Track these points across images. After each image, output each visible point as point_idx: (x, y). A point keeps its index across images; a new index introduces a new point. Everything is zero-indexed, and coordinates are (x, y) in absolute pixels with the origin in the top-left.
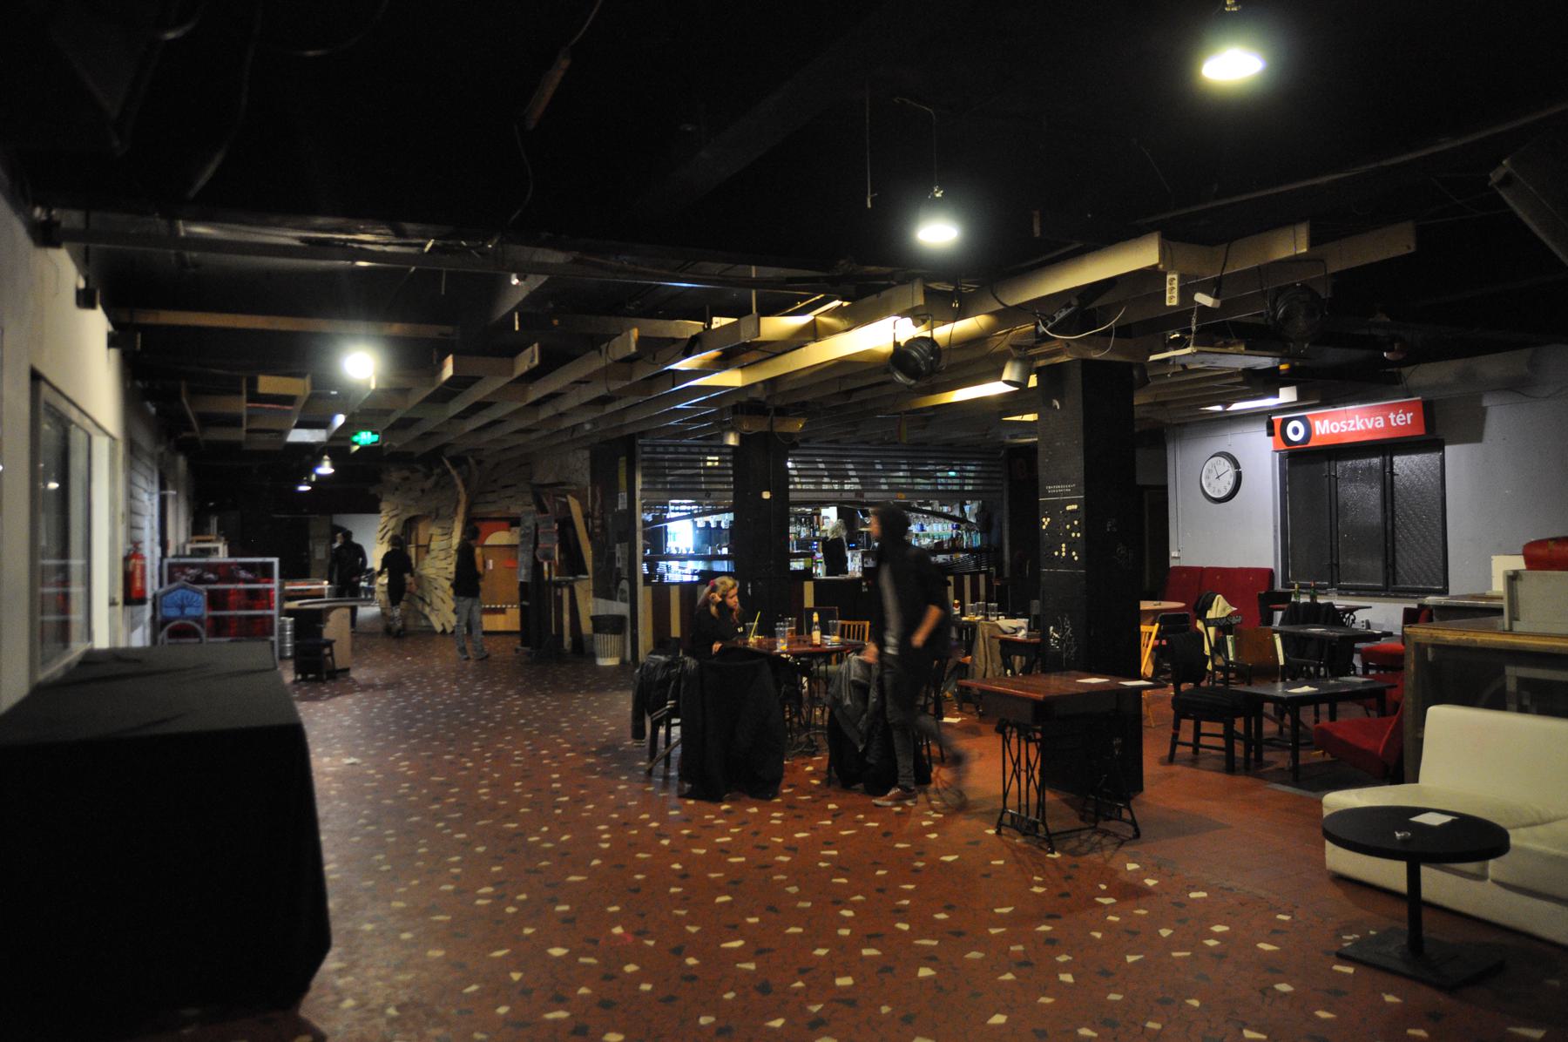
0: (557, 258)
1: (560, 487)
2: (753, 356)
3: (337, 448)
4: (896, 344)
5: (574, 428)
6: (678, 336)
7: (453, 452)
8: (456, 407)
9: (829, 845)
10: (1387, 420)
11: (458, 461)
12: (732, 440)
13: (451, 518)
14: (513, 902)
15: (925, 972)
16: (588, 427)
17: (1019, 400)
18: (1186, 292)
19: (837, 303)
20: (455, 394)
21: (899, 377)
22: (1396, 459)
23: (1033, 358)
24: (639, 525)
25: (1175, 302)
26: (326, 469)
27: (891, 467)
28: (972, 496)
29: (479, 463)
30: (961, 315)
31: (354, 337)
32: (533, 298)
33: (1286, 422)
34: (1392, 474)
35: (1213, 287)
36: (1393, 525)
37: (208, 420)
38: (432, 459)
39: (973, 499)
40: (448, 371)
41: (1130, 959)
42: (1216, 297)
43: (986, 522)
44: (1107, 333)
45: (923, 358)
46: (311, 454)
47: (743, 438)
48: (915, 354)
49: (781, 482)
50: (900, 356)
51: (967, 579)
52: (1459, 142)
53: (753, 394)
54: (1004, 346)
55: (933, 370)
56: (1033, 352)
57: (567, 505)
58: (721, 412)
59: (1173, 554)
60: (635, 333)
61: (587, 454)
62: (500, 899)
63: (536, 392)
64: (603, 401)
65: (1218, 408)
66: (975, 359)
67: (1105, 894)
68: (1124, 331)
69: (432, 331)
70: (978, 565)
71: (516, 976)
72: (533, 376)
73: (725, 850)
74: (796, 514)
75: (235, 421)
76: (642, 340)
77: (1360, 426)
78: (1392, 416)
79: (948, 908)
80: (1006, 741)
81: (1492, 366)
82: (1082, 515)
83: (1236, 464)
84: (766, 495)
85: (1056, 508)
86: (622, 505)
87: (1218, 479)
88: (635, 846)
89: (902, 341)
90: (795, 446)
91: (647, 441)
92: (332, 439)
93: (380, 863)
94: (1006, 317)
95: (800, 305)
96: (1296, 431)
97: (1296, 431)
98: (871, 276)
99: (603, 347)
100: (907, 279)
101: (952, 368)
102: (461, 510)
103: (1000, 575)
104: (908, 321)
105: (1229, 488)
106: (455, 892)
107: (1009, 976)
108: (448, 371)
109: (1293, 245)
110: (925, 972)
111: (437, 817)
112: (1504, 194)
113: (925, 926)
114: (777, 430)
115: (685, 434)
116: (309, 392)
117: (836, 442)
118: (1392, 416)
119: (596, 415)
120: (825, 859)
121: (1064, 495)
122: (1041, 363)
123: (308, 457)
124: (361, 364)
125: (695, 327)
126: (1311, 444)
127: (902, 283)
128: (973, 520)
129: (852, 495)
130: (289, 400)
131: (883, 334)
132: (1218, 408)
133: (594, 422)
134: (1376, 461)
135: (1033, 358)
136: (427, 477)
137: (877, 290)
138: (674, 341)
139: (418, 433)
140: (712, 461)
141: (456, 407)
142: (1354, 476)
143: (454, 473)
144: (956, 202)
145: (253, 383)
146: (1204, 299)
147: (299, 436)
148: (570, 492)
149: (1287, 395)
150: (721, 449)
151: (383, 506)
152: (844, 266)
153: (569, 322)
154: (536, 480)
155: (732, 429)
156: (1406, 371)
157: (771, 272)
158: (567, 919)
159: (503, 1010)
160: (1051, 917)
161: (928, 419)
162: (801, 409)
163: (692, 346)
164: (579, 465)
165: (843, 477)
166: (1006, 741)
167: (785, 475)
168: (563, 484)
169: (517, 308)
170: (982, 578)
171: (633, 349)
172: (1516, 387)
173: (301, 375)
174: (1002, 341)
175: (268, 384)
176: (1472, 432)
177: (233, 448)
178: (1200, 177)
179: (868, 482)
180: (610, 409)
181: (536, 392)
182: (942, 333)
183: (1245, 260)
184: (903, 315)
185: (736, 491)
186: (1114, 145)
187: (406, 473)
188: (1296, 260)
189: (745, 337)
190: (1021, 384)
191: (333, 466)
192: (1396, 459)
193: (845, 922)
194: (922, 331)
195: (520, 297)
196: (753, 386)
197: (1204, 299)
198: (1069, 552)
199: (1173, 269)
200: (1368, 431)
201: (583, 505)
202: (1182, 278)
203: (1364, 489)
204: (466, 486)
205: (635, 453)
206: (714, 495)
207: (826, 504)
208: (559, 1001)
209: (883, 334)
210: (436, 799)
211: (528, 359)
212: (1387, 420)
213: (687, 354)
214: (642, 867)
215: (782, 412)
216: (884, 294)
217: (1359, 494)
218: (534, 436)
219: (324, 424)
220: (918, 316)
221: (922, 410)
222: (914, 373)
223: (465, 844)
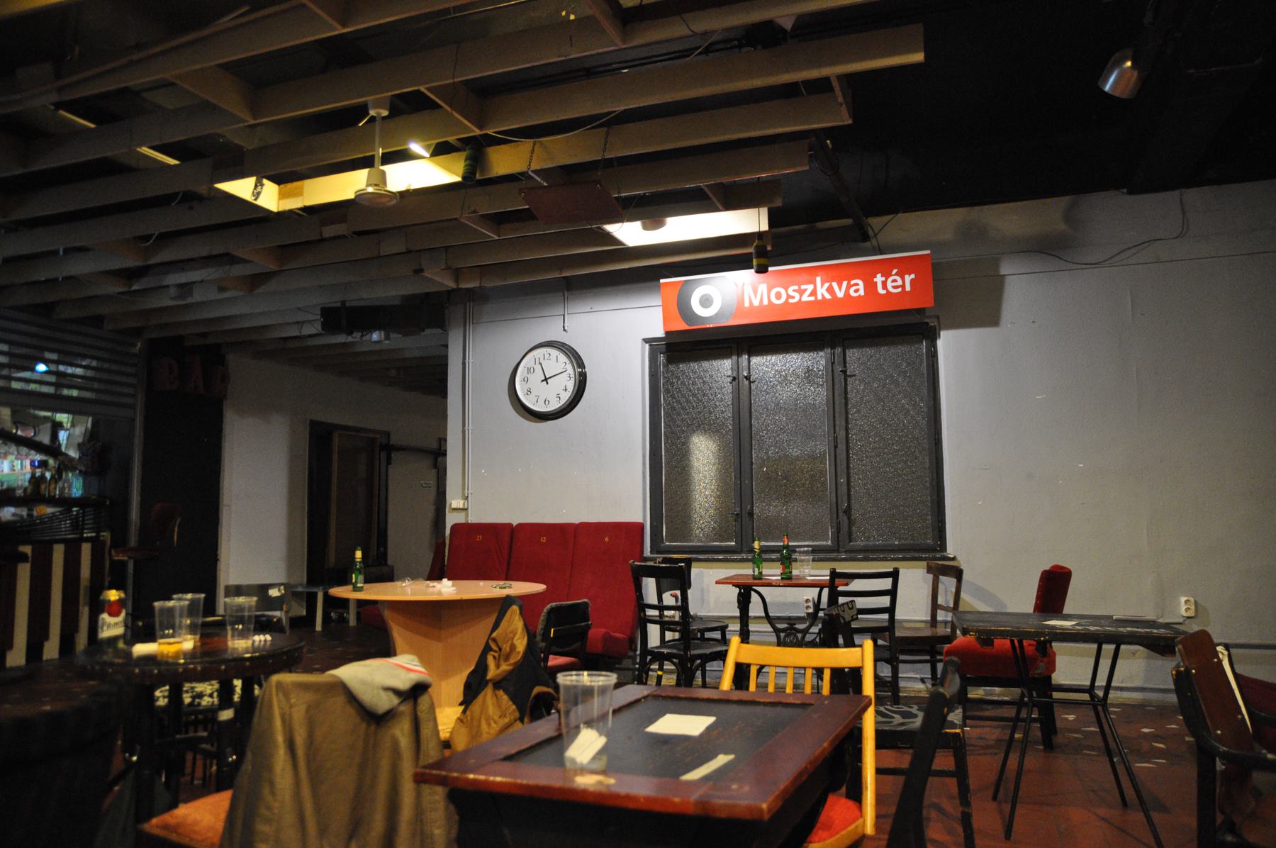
10: (870, 286)
43: (98, 456)
51: (58, 553)
70: (77, 526)
77: (822, 292)
78: (879, 279)
80: (796, 560)
81: (1008, 219)
103: (120, 542)
118: (879, 279)
128: (73, 454)
166: (796, 560)
170: (86, 549)
172: (1049, 248)
176: (984, 311)
212: (870, 286)
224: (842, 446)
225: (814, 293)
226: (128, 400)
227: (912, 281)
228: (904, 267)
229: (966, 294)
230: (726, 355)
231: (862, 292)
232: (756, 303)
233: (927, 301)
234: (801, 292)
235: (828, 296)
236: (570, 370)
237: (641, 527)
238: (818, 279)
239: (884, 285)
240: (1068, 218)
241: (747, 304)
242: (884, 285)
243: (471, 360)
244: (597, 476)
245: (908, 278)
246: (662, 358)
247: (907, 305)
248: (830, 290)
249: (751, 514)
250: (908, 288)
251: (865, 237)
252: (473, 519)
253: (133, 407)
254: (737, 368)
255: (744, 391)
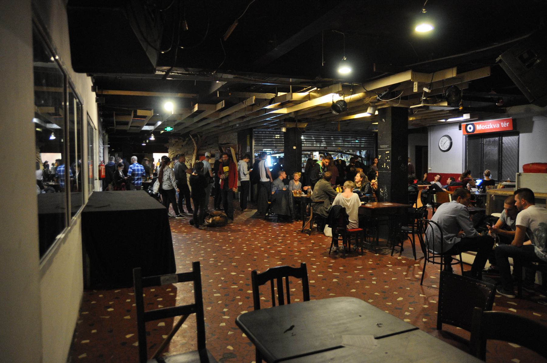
0: (230, 76)
1: (227, 145)
2: (291, 104)
3: (156, 132)
4: (333, 102)
5: (233, 126)
6: (267, 98)
7: (193, 133)
8: (196, 119)
9: (311, 251)
10: (500, 125)
11: (194, 136)
12: (284, 130)
13: (192, 155)
14: (220, 262)
15: (335, 280)
16: (237, 125)
17: (373, 118)
18: (420, 87)
19: (316, 88)
20: (197, 115)
21: (334, 112)
22: (504, 138)
23: (377, 106)
24: (253, 157)
25: (416, 91)
26: (152, 138)
27: (336, 139)
28: (364, 149)
29: (201, 136)
30: (354, 93)
31: (167, 97)
32: (223, 87)
33: (467, 125)
34: (502, 143)
35: (429, 86)
36: (502, 160)
37: (119, 123)
38: (186, 135)
39: (364, 150)
40: (196, 109)
41: (393, 279)
42: (429, 89)
44: (398, 99)
45: (341, 107)
46: (149, 133)
47: (287, 129)
48: (339, 105)
49: (299, 143)
50: (334, 106)
52: (500, 45)
53: (291, 116)
54: (368, 102)
55: (344, 110)
56: (376, 104)
57: (230, 150)
58: (280, 121)
59: (429, 168)
60: (254, 98)
61: (236, 134)
62: (216, 261)
63: (222, 115)
64: (243, 117)
65: (444, 121)
66: (359, 106)
67: (390, 264)
68: (404, 98)
69: (191, 96)
71: (223, 278)
72: (222, 110)
73: (280, 251)
74: (305, 154)
75: (126, 123)
76: (256, 99)
77: (491, 127)
78: (502, 124)
79: (343, 266)
82: (390, 155)
83: (450, 139)
84: (295, 148)
85: (383, 152)
86: (248, 151)
87: (444, 144)
88: (254, 250)
89: (335, 101)
90: (304, 132)
91: (256, 130)
92: (156, 129)
93: (181, 253)
94: (369, 93)
95: (305, 89)
96: (470, 128)
97: (470, 128)
98: (326, 82)
99: (244, 101)
100: (337, 82)
101: (353, 108)
102: (195, 152)
104: (338, 95)
105: (448, 147)
106: (204, 260)
107: (358, 282)
108: (196, 109)
109: (452, 74)
110: (335, 280)
111: (195, 242)
112: (501, 65)
113: (336, 269)
114: (298, 127)
115: (269, 128)
116: (153, 115)
117: (318, 130)
118: (502, 124)
119: (241, 121)
120: (309, 254)
121: (386, 148)
122: (379, 107)
123: (146, 135)
124: (169, 106)
125: (272, 95)
126: (475, 133)
127: (335, 84)
129: (323, 148)
130: (145, 117)
131: (331, 98)
132: (444, 121)
133: (239, 124)
134: (497, 139)
135: (377, 106)
136: (184, 141)
137: (328, 86)
138: (266, 100)
139: (183, 127)
140: (277, 136)
141: (196, 119)
142: (489, 144)
143: (193, 140)
144: (351, 60)
145: (135, 112)
146: (426, 90)
147: (146, 128)
148: (231, 146)
149: (466, 116)
150: (280, 133)
151: (169, 150)
152: (318, 78)
153: (233, 95)
154: (220, 142)
155: (284, 126)
156: (508, 108)
157: (295, 80)
158: (235, 266)
159: (220, 285)
160: (372, 269)
161: (348, 123)
162: (306, 120)
163: (271, 101)
164: (234, 138)
165: (321, 142)
167: (301, 142)
168: (229, 144)
169: (218, 90)
171: (254, 102)
173: (150, 110)
174: (368, 100)
175: (140, 112)
176: (529, 130)
177: (125, 131)
178: (420, 57)
179: (329, 143)
180: (245, 120)
181: (222, 115)
182: (348, 98)
183: (438, 77)
184: (337, 93)
185: (285, 146)
186: (385, 52)
187: (177, 140)
188: (453, 78)
189: (288, 99)
190: (373, 114)
191: (155, 138)
192: (504, 138)
193: (314, 269)
194: (342, 98)
195: (219, 86)
196: (290, 113)
197: (426, 90)
198: (386, 166)
199: (415, 81)
200: (494, 129)
201: (235, 150)
202: (419, 83)
203: (492, 148)
204: (197, 144)
205: (249, 133)
206: (278, 147)
207: (315, 151)
208: (235, 284)
209: (331, 98)
210: (194, 238)
211: (221, 105)
212: (500, 125)
213: (270, 104)
214: (256, 255)
215: (300, 121)
216: (330, 87)
217: (491, 150)
218: (221, 128)
219: (153, 124)
220: (341, 93)
221: (345, 120)
222: (338, 111)
223: (204, 249)
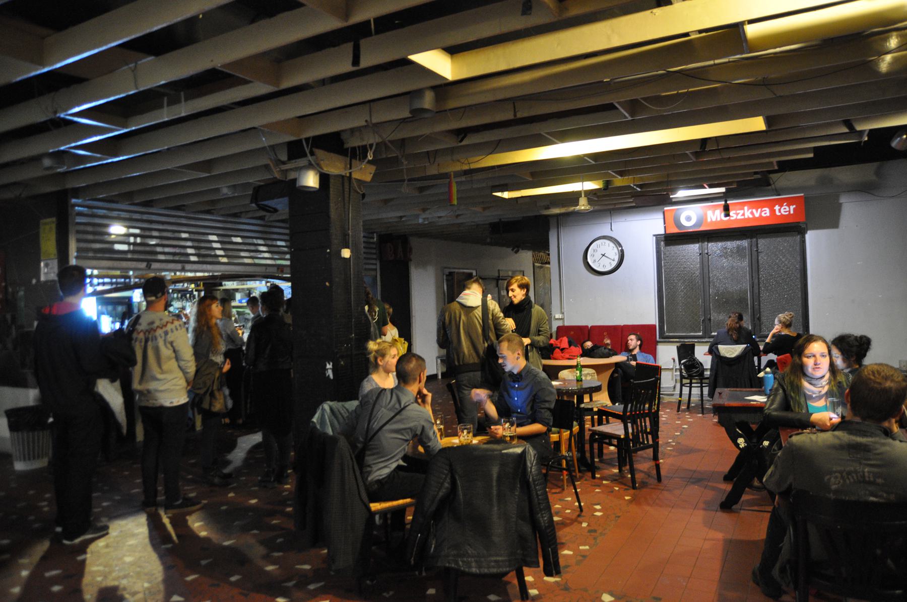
10: (773, 211)
77: (748, 214)
78: (777, 208)
118: (777, 208)
172: (866, 189)
176: (830, 220)
212: (773, 211)
224: (756, 287)
225: (743, 215)
226: (374, 267)
227: (794, 209)
228: (790, 202)
229: (820, 212)
230: (698, 242)
231: (768, 214)
232: (714, 220)
233: (801, 219)
234: (737, 214)
235: (751, 216)
236: (616, 249)
237: (655, 326)
238: (746, 208)
239: (780, 211)
240: (878, 173)
241: (709, 220)
242: (780, 211)
243: (562, 245)
244: (634, 301)
245: (792, 207)
246: (662, 243)
247: (791, 220)
248: (752, 213)
249: (710, 320)
250: (792, 212)
251: (769, 185)
252: (566, 324)
253: (376, 270)
254: (701, 248)
255: (705, 259)
